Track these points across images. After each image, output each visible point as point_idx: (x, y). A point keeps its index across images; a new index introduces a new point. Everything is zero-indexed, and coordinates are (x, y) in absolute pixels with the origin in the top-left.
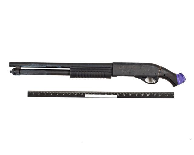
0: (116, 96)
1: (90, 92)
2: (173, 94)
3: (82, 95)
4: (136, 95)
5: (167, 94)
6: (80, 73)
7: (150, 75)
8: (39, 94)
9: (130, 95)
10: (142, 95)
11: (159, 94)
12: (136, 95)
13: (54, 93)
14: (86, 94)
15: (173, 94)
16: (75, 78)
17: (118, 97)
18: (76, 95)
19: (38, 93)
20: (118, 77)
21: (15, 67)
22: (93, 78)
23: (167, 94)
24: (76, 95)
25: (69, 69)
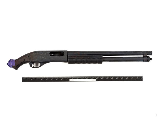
0: (95, 80)
1: (121, 76)
2: (142, 77)
3: (67, 79)
4: (112, 79)
5: (137, 77)
6: (92, 60)
7: (37, 60)
8: (32, 79)
9: (107, 79)
10: (117, 79)
11: (131, 77)
12: (112, 79)
13: (29, 78)
14: (71, 78)
15: (142, 77)
16: (72, 64)
17: (97, 81)
18: (62, 79)
19: (31, 79)
20: (47, 64)
21: (148, 56)
22: (75, 64)
23: (137, 77)
24: (62, 79)
25: (103, 56)
